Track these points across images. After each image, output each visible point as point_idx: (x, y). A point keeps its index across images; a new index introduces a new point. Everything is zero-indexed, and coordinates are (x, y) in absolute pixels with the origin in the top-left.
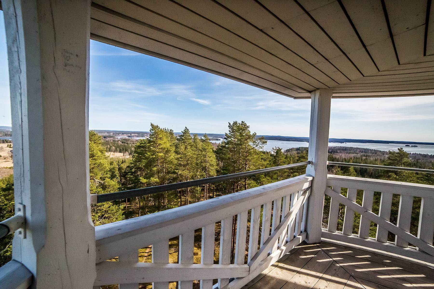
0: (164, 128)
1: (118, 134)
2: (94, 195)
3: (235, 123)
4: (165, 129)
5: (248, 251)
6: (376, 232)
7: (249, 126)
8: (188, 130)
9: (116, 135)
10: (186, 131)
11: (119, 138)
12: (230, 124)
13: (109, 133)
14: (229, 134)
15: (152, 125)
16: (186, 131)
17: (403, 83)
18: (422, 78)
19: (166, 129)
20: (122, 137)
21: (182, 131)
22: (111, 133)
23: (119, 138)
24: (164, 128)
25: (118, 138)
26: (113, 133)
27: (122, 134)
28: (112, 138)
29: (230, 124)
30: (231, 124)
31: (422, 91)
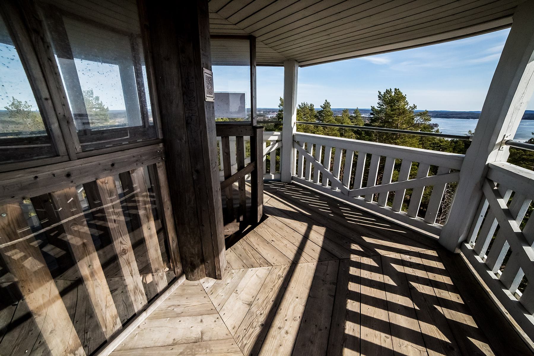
0: (303, 103)
1: (269, 112)
2: (138, 108)
3: (388, 92)
4: (304, 104)
5: (219, 147)
6: (423, 196)
7: (406, 95)
8: (328, 103)
9: (266, 114)
10: (327, 105)
11: (269, 116)
12: (380, 93)
13: (259, 111)
14: (378, 107)
15: (326, 101)
16: (327, 105)
17: (423, 26)
18: (412, 24)
19: (305, 103)
20: (272, 116)
21: (321, 106)
22: (261, 111)
23: (269, 116)
24: (303, 103)
25: (268, 117)
26: (264, 111)
27: (273, 112)
28: (262, 118)
29: (380, 93)
30: (382, 93)
31: (413, 41)
